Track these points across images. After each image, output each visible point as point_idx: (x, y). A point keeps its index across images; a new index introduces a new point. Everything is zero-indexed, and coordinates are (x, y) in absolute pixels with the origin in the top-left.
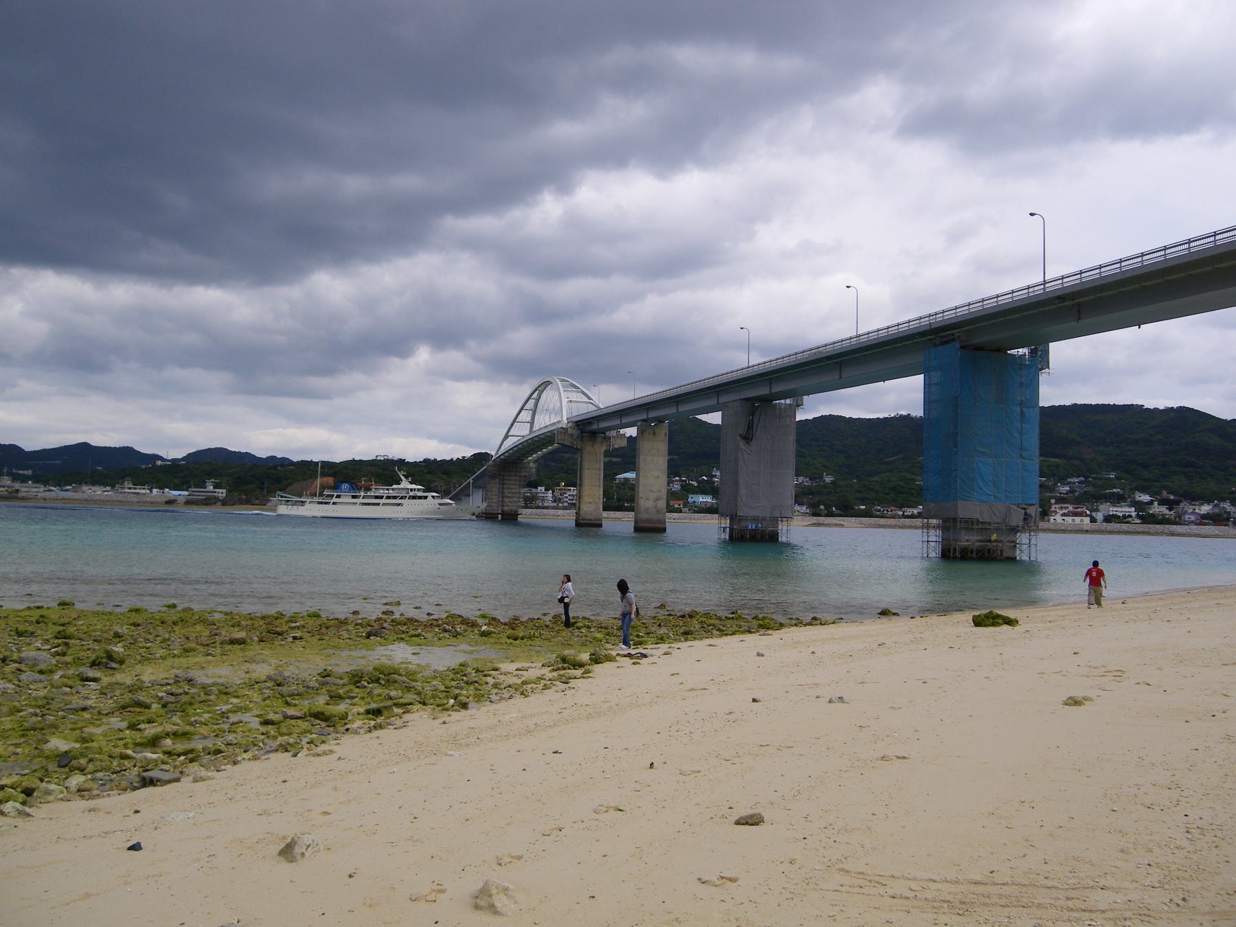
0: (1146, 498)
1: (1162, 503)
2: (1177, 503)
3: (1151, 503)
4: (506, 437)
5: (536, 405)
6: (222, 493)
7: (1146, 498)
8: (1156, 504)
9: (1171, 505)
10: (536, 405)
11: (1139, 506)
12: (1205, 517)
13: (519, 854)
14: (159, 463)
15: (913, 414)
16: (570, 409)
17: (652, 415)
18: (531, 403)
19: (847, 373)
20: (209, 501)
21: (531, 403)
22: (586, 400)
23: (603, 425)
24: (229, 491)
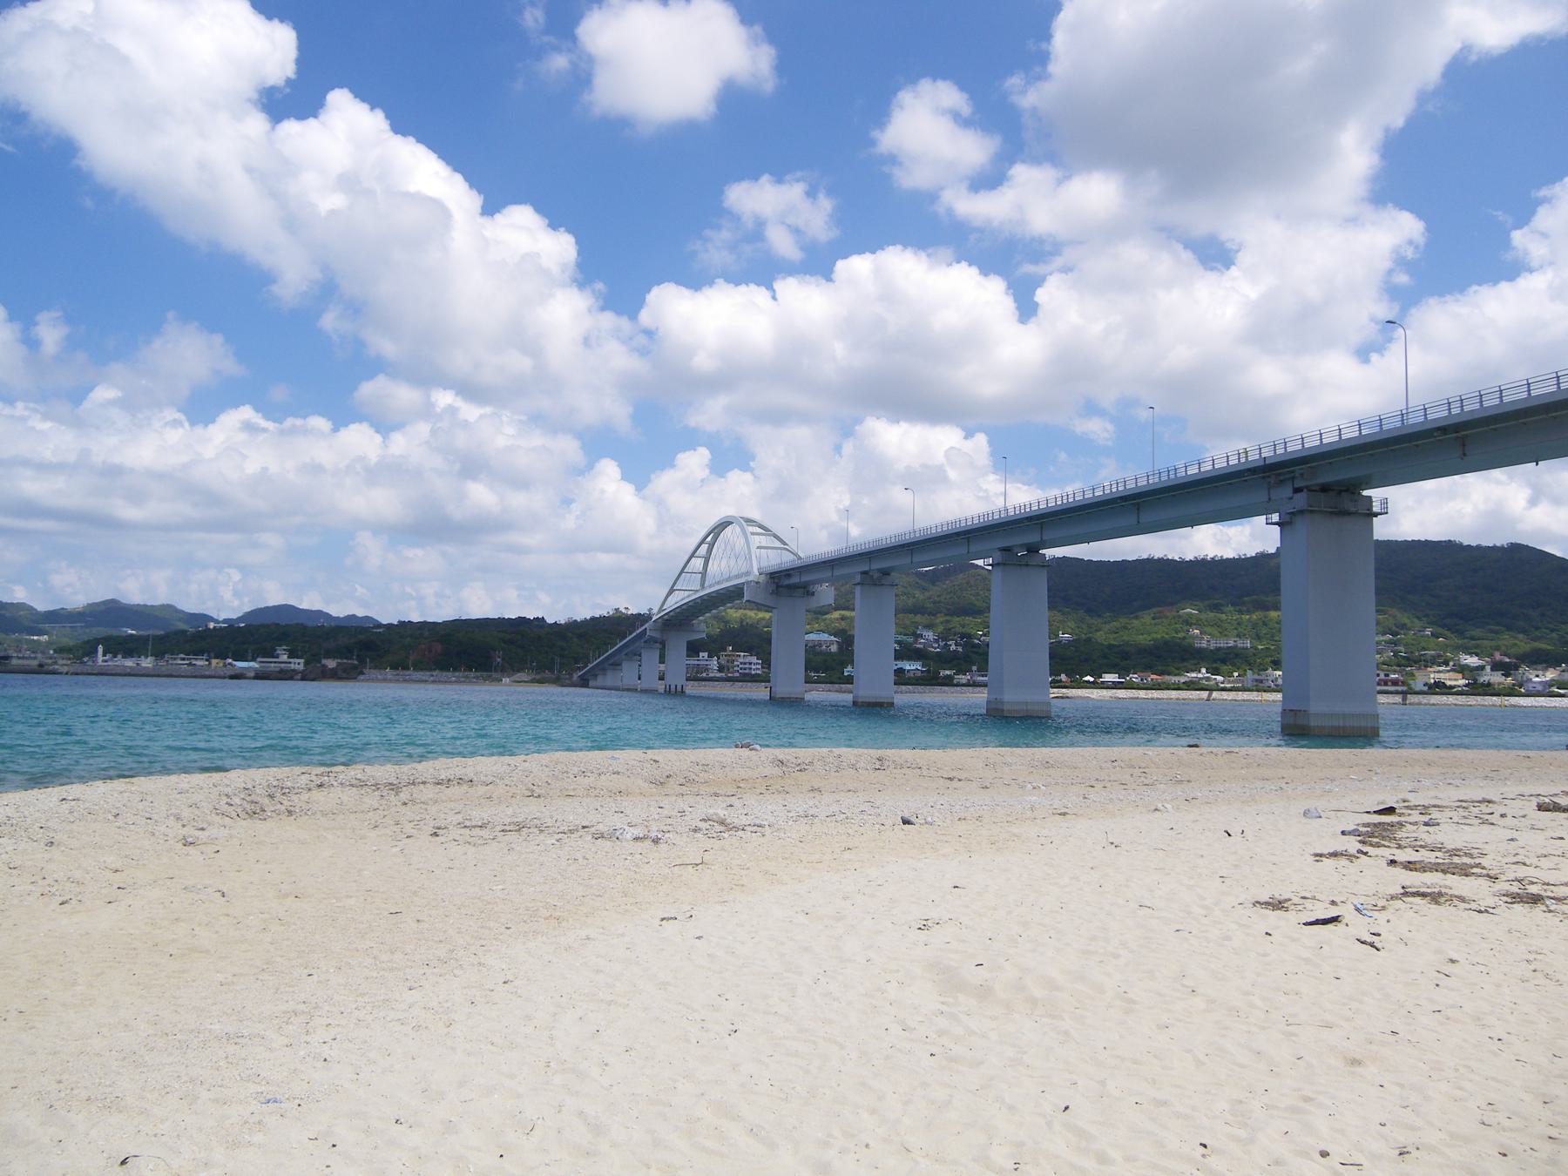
0: (1472, 661)
1: (1496, 667)
2: (1517, 668)
3: (1482, 668)
4: (671, 591)
5: (710, 551)
6: (298, 664)
7: (1472, 661)
8: (1488, 668)
9: (1506, 669)
10: (710, 551)
11: (1462, 670)
12: (1550, 684)
13: (1391, 869)
14: (212, 625)
15: (745, 185)
16: (759, 559)
17: (876, 565)
18: (704, 549)
19: (1146, 517)
20: (285, 675)
21: (704, 547)
22: (778, 544)
23: (806, 578)
24: (306, 664)
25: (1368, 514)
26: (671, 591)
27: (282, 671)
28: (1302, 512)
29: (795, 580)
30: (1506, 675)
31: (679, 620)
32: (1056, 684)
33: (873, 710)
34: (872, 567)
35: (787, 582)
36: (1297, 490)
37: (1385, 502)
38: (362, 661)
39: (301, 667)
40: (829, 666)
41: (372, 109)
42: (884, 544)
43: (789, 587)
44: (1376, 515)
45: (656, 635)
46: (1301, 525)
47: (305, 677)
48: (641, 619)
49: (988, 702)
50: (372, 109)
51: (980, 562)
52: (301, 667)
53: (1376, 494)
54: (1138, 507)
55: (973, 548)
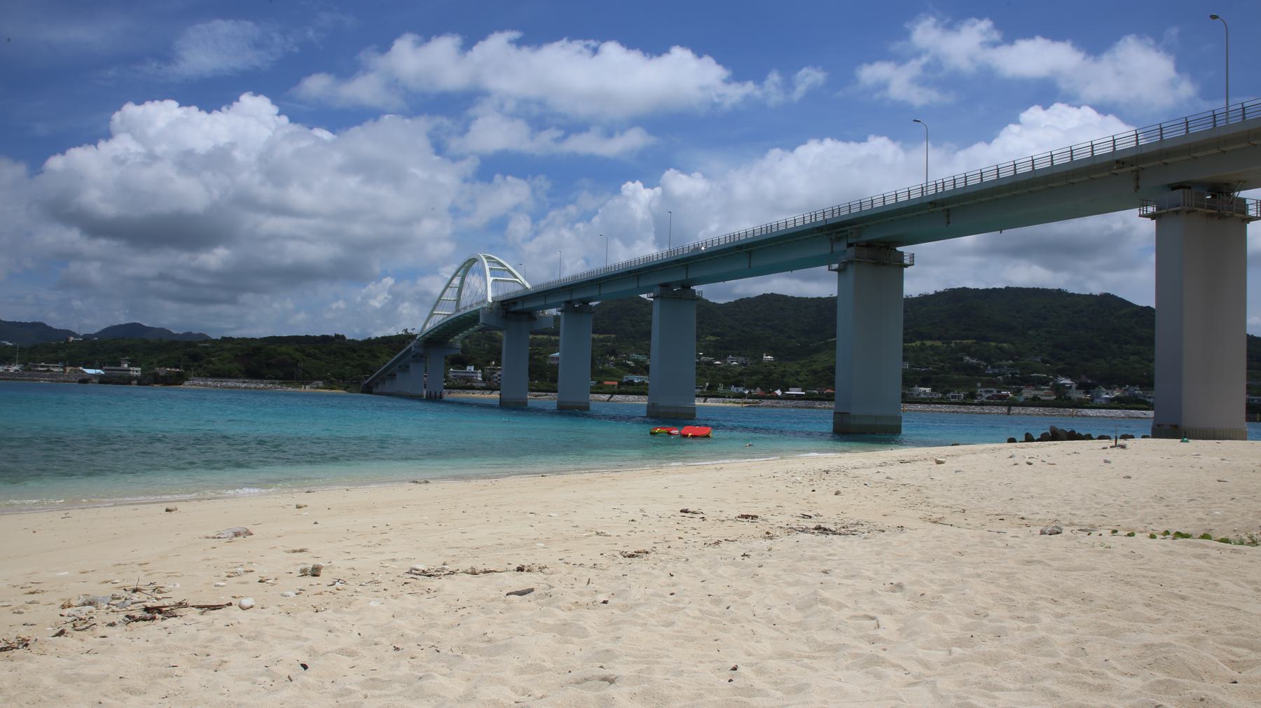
2: (1093, 386)
4: (431, 315)
5: (462, 282)
6: (136, 371)
17: (576, 296)
18: (456, 282)
23: (528, 305)
25: (899, 264)
26: (431, 315)
27: (120, 377)
28: (851, 262)
29: (519, 307)
30: (1087, 393)
31: (438, 339)
32: (599, 389)
33: (572, 410)
34: (574, 296)
35: (513, 309)
36: (850, 245)
37: (912, 256)
38: (187, 368)
39: (139, 374)
40: (543, 376)
41: (238, 101)
42: (552, 286)
43: (516, 313)
44: (906, 266)
45: (421, 351)
46: (851, 271)
47: (141, 382)
48: (406, 338)
49: (648, 406)
50: (238, 101)
51: (644, 296)
52: (139, 374)
53: (906, 250)
54: (750, 254)
55: (643, 284)
